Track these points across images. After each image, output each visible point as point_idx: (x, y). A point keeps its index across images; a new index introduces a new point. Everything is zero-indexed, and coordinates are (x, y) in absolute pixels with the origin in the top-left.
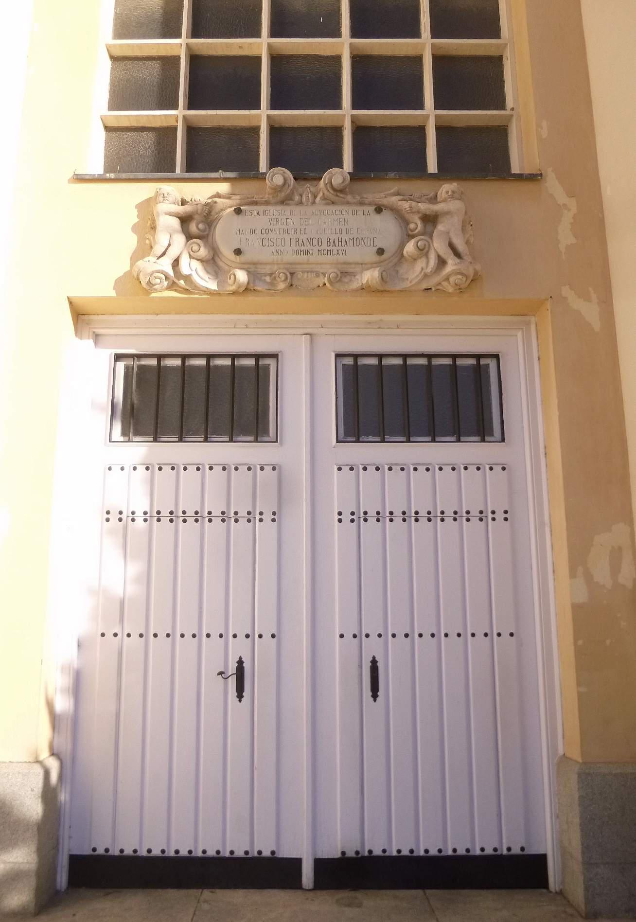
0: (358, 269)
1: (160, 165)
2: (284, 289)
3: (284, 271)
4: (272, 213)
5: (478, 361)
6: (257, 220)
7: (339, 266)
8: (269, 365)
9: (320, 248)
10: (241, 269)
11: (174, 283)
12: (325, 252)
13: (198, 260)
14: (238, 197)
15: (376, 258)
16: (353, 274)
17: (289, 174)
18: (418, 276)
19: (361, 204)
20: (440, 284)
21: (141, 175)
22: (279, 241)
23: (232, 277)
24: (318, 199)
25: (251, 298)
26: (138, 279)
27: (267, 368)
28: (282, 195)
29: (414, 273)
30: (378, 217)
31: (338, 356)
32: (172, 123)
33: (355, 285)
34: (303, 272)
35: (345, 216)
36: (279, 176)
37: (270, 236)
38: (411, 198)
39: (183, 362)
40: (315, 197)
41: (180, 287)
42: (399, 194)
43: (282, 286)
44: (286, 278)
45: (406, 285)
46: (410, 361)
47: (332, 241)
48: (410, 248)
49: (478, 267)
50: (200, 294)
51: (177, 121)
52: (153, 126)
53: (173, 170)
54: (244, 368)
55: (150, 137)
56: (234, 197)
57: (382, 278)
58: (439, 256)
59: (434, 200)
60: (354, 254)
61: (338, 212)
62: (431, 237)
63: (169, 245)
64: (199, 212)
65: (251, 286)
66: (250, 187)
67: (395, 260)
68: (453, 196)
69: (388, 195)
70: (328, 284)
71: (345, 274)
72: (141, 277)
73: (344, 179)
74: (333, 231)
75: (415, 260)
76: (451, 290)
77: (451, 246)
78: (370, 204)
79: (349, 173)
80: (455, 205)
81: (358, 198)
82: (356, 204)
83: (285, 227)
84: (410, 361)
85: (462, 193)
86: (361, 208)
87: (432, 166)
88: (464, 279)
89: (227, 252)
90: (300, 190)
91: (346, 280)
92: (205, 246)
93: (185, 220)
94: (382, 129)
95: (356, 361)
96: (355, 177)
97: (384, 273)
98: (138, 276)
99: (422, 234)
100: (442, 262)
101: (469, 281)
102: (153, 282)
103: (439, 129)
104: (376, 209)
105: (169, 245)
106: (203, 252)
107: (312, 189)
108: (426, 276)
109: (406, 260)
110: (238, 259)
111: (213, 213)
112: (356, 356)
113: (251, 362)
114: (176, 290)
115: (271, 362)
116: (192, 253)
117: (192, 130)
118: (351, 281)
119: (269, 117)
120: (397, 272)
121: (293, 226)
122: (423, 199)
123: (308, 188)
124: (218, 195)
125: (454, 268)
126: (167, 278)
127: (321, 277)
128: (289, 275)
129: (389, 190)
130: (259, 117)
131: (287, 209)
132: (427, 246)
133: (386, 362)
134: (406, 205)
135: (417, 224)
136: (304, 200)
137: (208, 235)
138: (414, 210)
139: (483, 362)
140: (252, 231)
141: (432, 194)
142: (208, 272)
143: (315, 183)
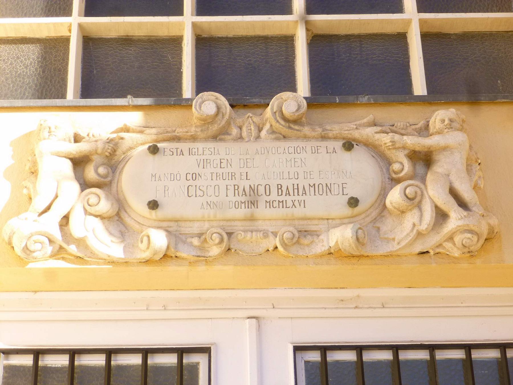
0: (322, 226)
1: (48, 87)
2: (220, 255)
3: (220, 231)
4: (200, 152)
5: (469, 354)
6: (180, 161)
7: (296, 222)
8: (198, 363)
9: (268, 199)
10: (159, 228)
11: (61, 248)
12: (276, 204)
13: (96, 216)
14: (154, 131)
15: (348, 211)
16: (315, 234)
17: (223, 101)
18: (408, 234)
19: (324, 138)
20: (440, 245)
21: (19, 103)
22: (211, 191)
23: (145, 239)
24: (263, 133)
25: (172, 269)
26: (10, 243)
27: (194, 368)
28: (215, 128)
29: (404, 230)
30: (347, 155)
31: (297, 349)
32: (64, 33)
33: (320, 248)
34: (245, 231)
35: (303, 155)
36: (211, 103)
37: (198, 182)
38: (392, 130)
39: (72, 360)
40: (260, 130)
41: (71, 255)
42: (375, 125)
43: (215, 251)
44: (222, 241)
45: (393, 247)
46: (440, 355)
47: (284, 189)
48: (395, 196)
49: (494, 221)
50: (98, 264)
51: (70, 31)
52: (37, 36)
53: (63, 96)
54: (160, 369)
55: (32, 53)
56: (148, 131)
57: (358, 239)
58: (436, 207)
59: (425, 131)
60: (316, 206)
61: (291, 150)
62: (423, 180)
63: (56, 197)
64: (99, 151)
65: (172, 252)
66: (170, 118)
67: (374, 214)
68: (451, 125)
69: (360, 125)
70: (280, 248)
71: (304, 233)
72: (15, 242)
73: (299, 107)
74: (286, 175)
75: (403, 212)
76: (456, 253)
77: (454, 193)
78: (335, 138)
79: (305, 98)
80: (455, 138)
81: (319, 130)
82: (316, 138)
83: (220, 171)
84: (440, 355)
85: (463, 121)
86: (324, 144)
87: (419, 86)
88: (475, 238)
89: (138, 206)
90: (239, 121)
91: (305, 241)
92: (107, 198)
93: (79, 163)
94: (348, 37)
95: (324, 356)
96: (312, 102)
97: (360, 231)
98: (10, 239)
99: (411, 178)
100: (441, 216)
101: (482, 241)
102: (32, 247)
103: (426, 37)
104: (344, 145)
105: (56, 197)
106: (104, 206)
107: (255, 119)
108: (420, 234)
109: (390, 213)
110: (154, 214)
111: (117, 153)
112: (324, 350)
113: (171, 360)
114: (63, 259)
115: (201, 359)
116: (88, 208)
117: (89, 42)
118: (312, 242)
119: (194, 25)
120: (379, 228)
121: (230, 170)
122: (410, 130)
123: (249, 119)
124: (126, 130)
125: (460, 223)
126: (51, 241)
127: (271, 237)
128: (225, 236)
129: (360, 120)
130: (181, 25)
131: (221, 147)
132: (419, 192)
133: (369, 356)
134: (385, 139)
135: (403, 165)
136: (245, 134)
137: (111, 182)
138: (397, 145)
139: (188, 359)
140: (174, 177)
141: (421, 123)
142: (111, 234)
143: (259, 111)
